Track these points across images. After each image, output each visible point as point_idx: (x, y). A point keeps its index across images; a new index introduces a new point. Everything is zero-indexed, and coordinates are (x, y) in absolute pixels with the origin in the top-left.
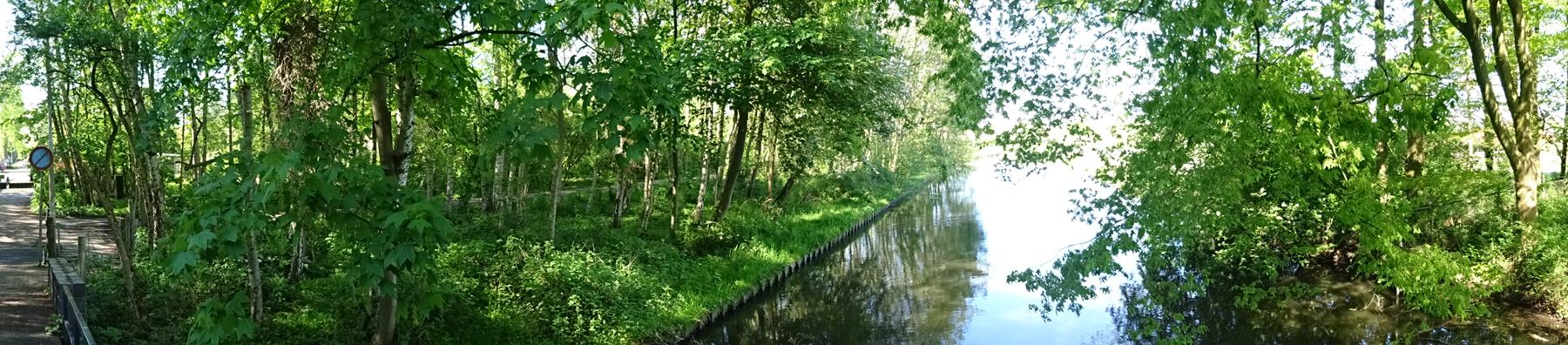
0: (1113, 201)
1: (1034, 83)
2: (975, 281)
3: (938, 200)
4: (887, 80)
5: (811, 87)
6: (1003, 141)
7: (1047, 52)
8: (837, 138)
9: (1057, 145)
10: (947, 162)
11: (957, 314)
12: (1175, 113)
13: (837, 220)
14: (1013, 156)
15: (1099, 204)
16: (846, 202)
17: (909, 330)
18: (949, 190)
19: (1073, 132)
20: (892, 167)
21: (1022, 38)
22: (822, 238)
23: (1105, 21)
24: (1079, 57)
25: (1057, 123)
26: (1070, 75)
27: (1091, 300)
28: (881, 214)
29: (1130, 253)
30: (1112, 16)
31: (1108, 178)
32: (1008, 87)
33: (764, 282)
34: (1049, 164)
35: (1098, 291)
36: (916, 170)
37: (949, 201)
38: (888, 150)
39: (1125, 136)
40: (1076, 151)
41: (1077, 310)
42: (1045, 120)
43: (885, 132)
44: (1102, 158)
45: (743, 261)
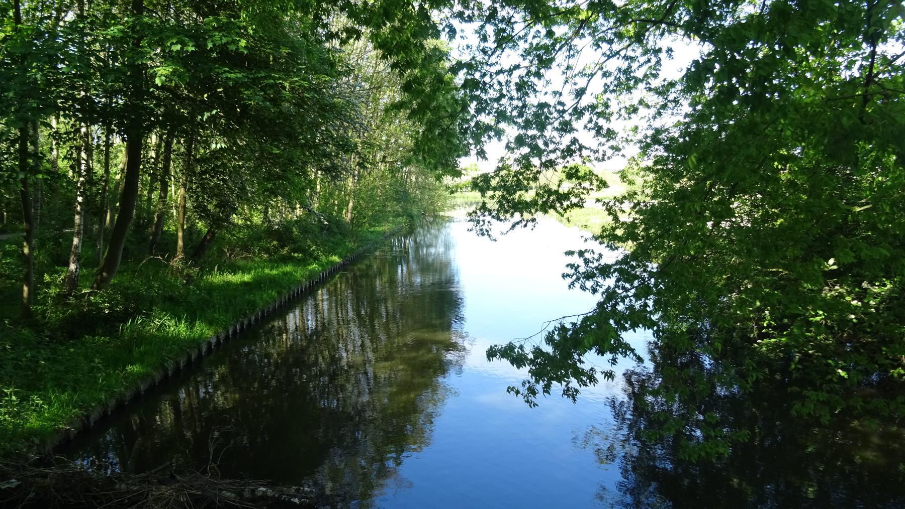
0: (625, 271)
1: (521, 115)
2: (450, 356)
3: (403, 257)
4: (333, 106)
5: (237, 116)
6: (481, 184)
7: (538, 75)
8: (270, 177)
9: (550, 192)
10: (415, 211)
11: (426, 395)
12: (710, 156)
13: (273, 282)
14: (492, 205)
15: (605, 271)
16: (285, 260)
17: (368, 414)
18: (418, 246)
19: (570, 176)
20: (347, 216)
21: (510, 57)
22: (252, 305)
23: (620, 36)
24: (582, 82)
25: (550, 164)
26: (569, 101)
27: (591, 387)
28: (332, 274)
29: (640, 330)
30: (631, 29)
31: (615, 238)
32: (487, 119)
33: (170, 365)
34: (539, 215)
35: (599, 376)
36: (376, 219)
37: (419, 259)
38: (341, 192)
39: (639, 181)
40: (574, 200)
41: (571, 394)
42: (535, 161)
43: (333, 172)
44: (610, 211)
45: (140, 339)
